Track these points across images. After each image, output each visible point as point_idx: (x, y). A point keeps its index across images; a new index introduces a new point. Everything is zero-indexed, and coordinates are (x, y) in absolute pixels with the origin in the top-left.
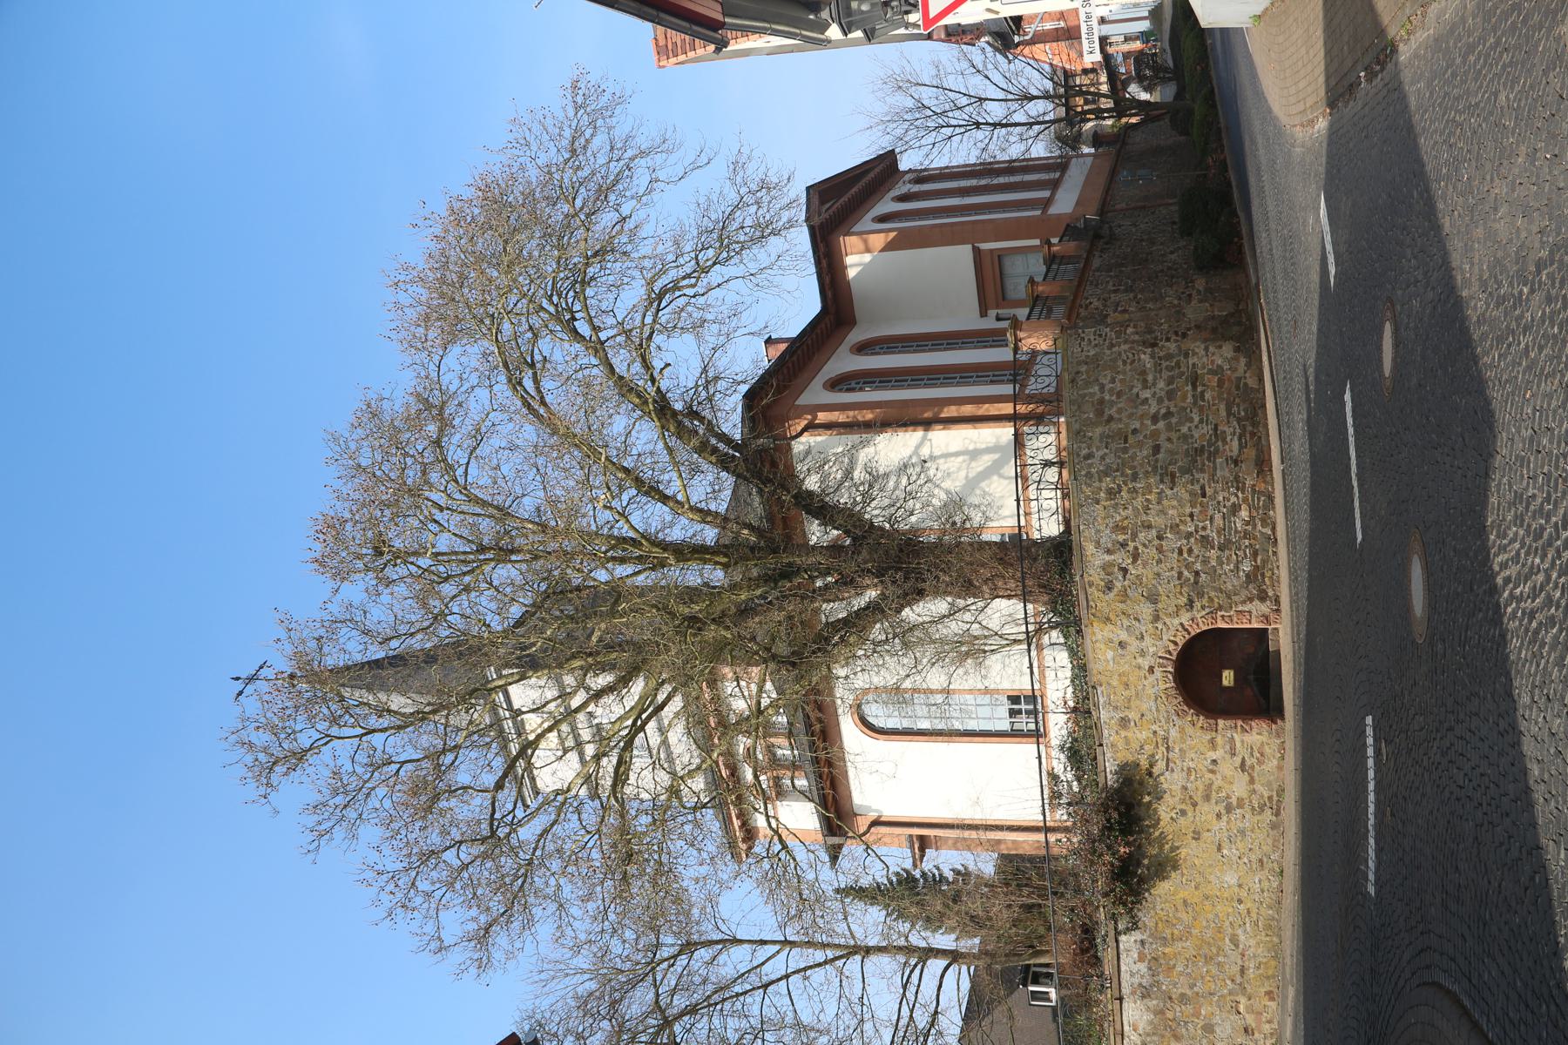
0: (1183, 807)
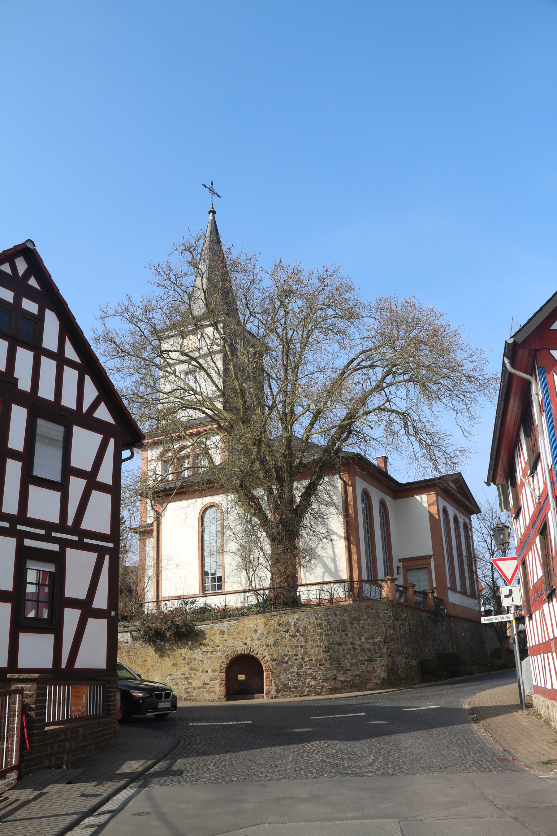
0: (187, 659)
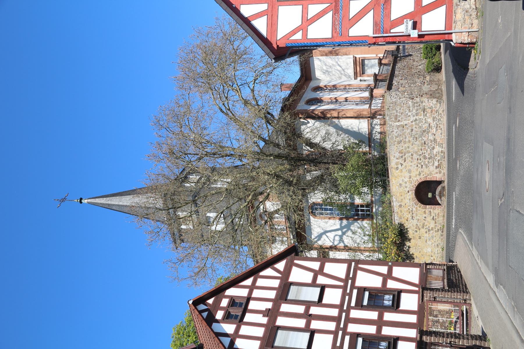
0: (416, 230)
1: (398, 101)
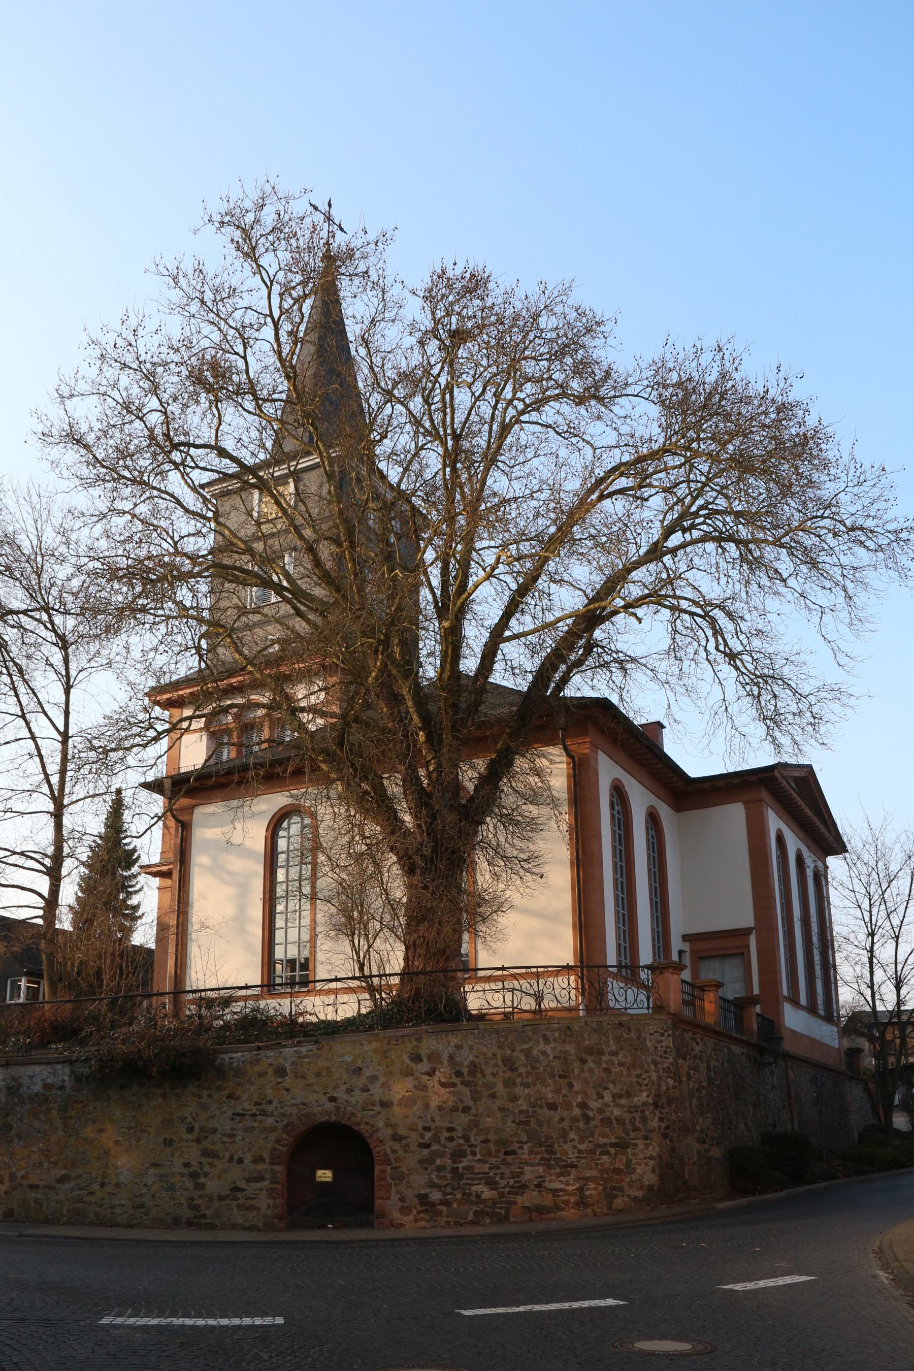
0: (197, 1129)
1: (648, 1056)
